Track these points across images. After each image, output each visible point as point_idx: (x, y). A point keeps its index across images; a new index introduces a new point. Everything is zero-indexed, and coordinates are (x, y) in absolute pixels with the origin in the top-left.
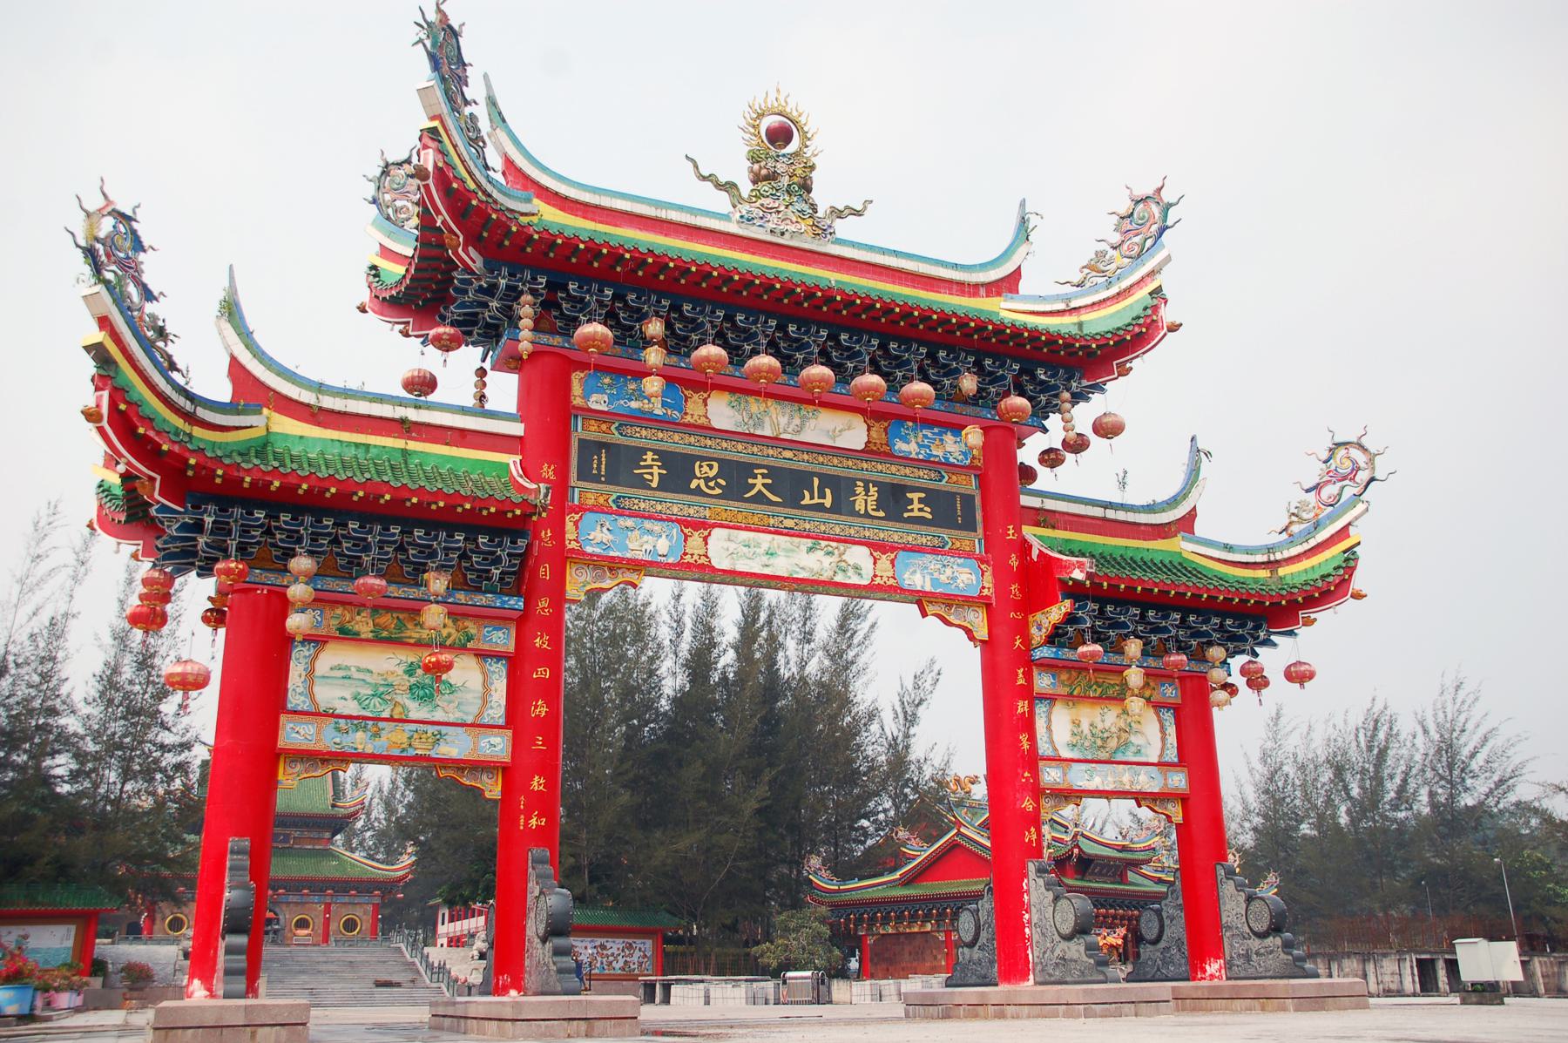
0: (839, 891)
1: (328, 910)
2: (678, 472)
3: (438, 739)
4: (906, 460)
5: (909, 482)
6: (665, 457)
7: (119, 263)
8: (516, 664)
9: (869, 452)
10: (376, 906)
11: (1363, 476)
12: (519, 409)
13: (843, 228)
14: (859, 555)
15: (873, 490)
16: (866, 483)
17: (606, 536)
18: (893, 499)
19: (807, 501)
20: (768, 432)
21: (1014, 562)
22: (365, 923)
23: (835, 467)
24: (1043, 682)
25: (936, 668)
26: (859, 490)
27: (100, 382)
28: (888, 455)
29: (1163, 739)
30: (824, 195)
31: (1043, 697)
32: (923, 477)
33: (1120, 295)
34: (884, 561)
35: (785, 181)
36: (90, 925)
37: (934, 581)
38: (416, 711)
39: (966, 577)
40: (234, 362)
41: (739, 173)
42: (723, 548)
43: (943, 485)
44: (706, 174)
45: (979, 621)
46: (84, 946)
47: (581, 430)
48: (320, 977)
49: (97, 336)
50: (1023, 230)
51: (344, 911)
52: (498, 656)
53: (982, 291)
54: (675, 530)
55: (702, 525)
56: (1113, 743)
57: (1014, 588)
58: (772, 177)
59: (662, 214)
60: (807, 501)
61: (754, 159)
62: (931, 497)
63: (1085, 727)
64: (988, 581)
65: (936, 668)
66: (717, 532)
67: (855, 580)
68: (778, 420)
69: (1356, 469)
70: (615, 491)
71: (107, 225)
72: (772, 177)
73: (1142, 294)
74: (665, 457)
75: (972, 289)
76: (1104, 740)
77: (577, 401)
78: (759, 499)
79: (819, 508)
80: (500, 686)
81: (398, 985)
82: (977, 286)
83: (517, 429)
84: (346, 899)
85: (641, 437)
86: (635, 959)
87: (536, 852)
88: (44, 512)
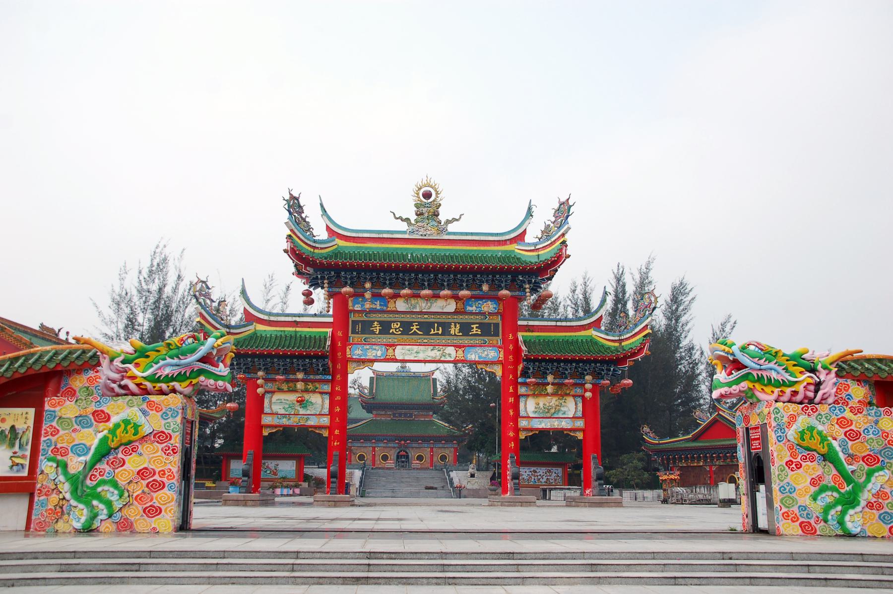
0: (659, 444)
1: (432, 451)
2: (385, 328)
3: (307, 419)
4: (471, 313)
5: (469, 321)
6: (381, 323)
7: (204, 295)
8: (332, 395)
9: (456, 312)
10: (456, 449)
11: (653, 305)
13: (451, 228)
14: (451, 350)
15: (458, 326)
16: (455, 323)
17: (360, 352)
18: (465, 329)
19: (432, 332)
20: (418, 310)
21: (511, 347)
22: (450, 458)
23: (443, 319)
24: (522, 390)
25: (732, 320)
28: (465, 313)
29: (576, 408)
30: (442, 217)
31: (523, 395)
32: (479, 319)
33: (552, 244)
34: (460, 351)
35: (426, 215)
36: (301, 461)
38: (302, 411)
40: (327, 226)
41: (413, 217)
42: (400, 352)
43: (487, 321)
44: (397, 216)
46: (300, 469)
47: (352, 317)
48: (402, 484)
49: (289, 233)
50: (530, 213)
51: (440, 451)
52: (326, 393)
53: (508, 242)
54: (384, 348)
55: (393, 346)
56: (553, 411)
57: (511, 357)
58: (422, 214)
59: (381, 236)
60: (432, 332)
61: (416, 206)
62: (481, 326)
63: (541, 405)
64: (502, 355)
65: (732, 320)
67: (449, 359)
68: (421, 305)
70: (365, 336)
71: (199, 287)
72: (422, 214)
73: (558, 243)
74: (381, 323)
75: (504, 243)
76: (549, 410)
77: (351, 308)
78: (415, 333)
79: (437, 334)
80: (327, 402)
81: (436, 488)
82: (506, 240)
83: (331, 320)
84: (441, 445)
86: (552, 477)
88: (268, 280)
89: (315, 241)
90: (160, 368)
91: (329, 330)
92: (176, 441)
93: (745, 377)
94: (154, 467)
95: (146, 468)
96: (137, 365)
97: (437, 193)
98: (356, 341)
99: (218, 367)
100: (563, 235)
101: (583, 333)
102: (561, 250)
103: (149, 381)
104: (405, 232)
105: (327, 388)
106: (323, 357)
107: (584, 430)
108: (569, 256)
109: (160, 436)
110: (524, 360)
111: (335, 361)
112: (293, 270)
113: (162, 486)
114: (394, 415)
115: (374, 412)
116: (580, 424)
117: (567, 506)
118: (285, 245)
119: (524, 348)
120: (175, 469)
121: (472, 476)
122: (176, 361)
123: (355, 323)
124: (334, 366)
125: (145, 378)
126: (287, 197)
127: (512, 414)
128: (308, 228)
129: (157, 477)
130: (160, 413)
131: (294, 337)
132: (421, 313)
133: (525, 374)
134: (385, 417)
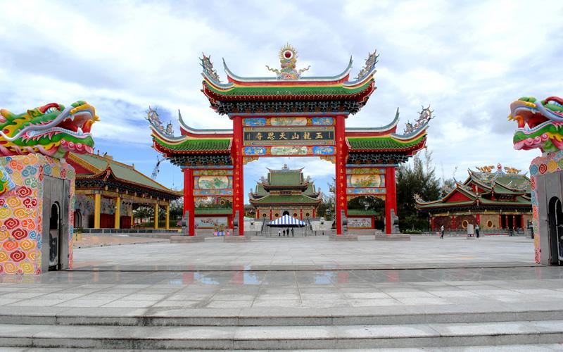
2: (265, 136)
6: (262, 133)
8: (234, 177)
9: (308, 125)
11: (428, 117)
12: (234, 127)
15: (309, 134)
18: (313, 135)
20: (284, 125)
21: (341, 146)
26: (305, 134)
27: (154, 141)
28: (312, 126)
31: (349, 175)
37: (322, 152)
38: (217, 187)
39: (329, 150)
40: (228, 76)
41: (280, 69)
45: (334, 159)
47: (244, 130)
62: (323, 133)
63: (360, 180)
66: (273, 148)
69: (426, 117)
70: (252, 142)
74: (262, 133)
78: (283, 139)
79: (296, 139)
83: (232, 132)
85: (257, 130)
87: (143, 220)
89: (221, 85)
90: (25, 133)
91: (231, 139)
92: (36, 195)
93: (547, 129)
94: (17, 218)
95: (11, 219)
96: (6, 132)
97: (294, 54)
98: (247, 144)
99: (76, 131)
100: (372, 75)
101: (385, 136)
102: (371, 84)
103: (18, 145)
104: (275, 78)
105: (231, 173)
106: (228, 154)
107: (386, 195)
108: (375, 88)
109: (24, 191)
110: (349, 153)
111: (235, 157)
112: (210, 104)
113: (25, 234)
114: (281, 193)
115: (271, 192)
116: (384, 191)
117: (376, 240)
118: (202, 87)
119: (349, 145)
120: (34, 219)
121: (322, 223)
122: (38, 126)
123: (246, 134)
124: (235, 160)
125: (13, 142)
126: (202, 58)
127: (342, 185)
128: (216, 76)
129: (20, 227)
130: (22, 171)
131: (209, 143)
132: (286, 126)
133: (349, 162)
134: (276, 193)
